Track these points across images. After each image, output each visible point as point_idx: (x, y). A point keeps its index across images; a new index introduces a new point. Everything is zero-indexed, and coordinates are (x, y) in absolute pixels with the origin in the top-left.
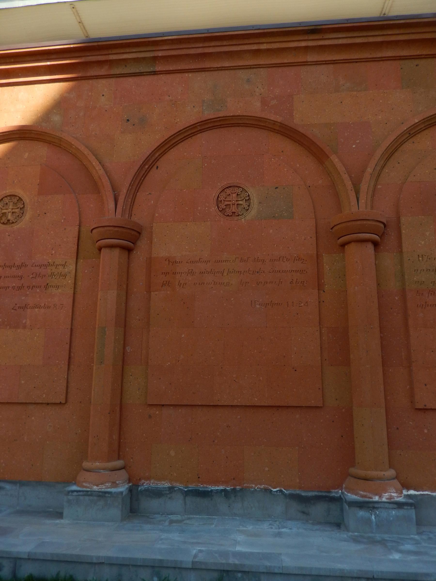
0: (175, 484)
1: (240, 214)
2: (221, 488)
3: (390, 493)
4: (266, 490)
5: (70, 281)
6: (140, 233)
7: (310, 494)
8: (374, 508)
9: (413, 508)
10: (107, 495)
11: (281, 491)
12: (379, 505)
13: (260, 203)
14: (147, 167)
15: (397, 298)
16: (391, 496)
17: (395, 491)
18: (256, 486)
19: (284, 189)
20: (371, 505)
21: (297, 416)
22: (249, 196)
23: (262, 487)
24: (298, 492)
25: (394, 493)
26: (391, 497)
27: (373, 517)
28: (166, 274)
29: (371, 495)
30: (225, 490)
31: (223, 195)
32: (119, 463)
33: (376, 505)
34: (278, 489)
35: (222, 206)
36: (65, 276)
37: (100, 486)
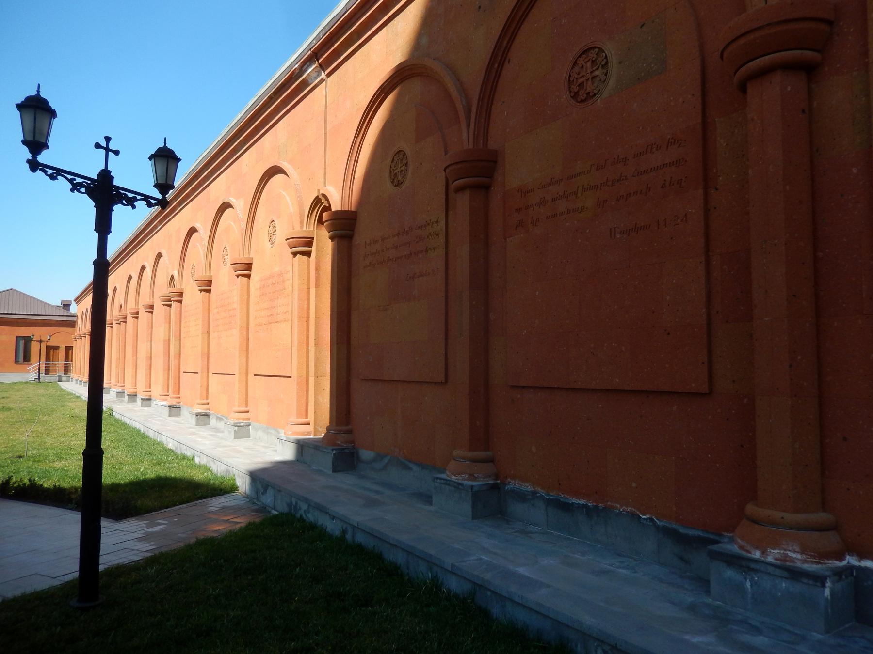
0: (539, 489)
1: (596, 92)
3: (785, 550)
4: (633, 515)
5: (442, 240)
6: (495, 162)
8: (751, 569)
9: (819, 584)
11: (651, 520)
12: (757, 567)
13: (620, 63)
14: (496, 66)
15: (855, 171)
16: (786, 555)
17: (798, 549)
18: (621, 506)
19: (653, 22)
20: (744, 563)
21: (674, 408)
23: (629, 509)
24: (674, 526)
25: (795, 552)
26: (785, 558)
27: (748, 584)
28: (519, 210)
29: (749, 548)
31: (576, 69)
32: (345, 428)
33: (753, 566)
34: (648, 516)
35: (575, 88)
36: (438, 235)
37: (457, 477)
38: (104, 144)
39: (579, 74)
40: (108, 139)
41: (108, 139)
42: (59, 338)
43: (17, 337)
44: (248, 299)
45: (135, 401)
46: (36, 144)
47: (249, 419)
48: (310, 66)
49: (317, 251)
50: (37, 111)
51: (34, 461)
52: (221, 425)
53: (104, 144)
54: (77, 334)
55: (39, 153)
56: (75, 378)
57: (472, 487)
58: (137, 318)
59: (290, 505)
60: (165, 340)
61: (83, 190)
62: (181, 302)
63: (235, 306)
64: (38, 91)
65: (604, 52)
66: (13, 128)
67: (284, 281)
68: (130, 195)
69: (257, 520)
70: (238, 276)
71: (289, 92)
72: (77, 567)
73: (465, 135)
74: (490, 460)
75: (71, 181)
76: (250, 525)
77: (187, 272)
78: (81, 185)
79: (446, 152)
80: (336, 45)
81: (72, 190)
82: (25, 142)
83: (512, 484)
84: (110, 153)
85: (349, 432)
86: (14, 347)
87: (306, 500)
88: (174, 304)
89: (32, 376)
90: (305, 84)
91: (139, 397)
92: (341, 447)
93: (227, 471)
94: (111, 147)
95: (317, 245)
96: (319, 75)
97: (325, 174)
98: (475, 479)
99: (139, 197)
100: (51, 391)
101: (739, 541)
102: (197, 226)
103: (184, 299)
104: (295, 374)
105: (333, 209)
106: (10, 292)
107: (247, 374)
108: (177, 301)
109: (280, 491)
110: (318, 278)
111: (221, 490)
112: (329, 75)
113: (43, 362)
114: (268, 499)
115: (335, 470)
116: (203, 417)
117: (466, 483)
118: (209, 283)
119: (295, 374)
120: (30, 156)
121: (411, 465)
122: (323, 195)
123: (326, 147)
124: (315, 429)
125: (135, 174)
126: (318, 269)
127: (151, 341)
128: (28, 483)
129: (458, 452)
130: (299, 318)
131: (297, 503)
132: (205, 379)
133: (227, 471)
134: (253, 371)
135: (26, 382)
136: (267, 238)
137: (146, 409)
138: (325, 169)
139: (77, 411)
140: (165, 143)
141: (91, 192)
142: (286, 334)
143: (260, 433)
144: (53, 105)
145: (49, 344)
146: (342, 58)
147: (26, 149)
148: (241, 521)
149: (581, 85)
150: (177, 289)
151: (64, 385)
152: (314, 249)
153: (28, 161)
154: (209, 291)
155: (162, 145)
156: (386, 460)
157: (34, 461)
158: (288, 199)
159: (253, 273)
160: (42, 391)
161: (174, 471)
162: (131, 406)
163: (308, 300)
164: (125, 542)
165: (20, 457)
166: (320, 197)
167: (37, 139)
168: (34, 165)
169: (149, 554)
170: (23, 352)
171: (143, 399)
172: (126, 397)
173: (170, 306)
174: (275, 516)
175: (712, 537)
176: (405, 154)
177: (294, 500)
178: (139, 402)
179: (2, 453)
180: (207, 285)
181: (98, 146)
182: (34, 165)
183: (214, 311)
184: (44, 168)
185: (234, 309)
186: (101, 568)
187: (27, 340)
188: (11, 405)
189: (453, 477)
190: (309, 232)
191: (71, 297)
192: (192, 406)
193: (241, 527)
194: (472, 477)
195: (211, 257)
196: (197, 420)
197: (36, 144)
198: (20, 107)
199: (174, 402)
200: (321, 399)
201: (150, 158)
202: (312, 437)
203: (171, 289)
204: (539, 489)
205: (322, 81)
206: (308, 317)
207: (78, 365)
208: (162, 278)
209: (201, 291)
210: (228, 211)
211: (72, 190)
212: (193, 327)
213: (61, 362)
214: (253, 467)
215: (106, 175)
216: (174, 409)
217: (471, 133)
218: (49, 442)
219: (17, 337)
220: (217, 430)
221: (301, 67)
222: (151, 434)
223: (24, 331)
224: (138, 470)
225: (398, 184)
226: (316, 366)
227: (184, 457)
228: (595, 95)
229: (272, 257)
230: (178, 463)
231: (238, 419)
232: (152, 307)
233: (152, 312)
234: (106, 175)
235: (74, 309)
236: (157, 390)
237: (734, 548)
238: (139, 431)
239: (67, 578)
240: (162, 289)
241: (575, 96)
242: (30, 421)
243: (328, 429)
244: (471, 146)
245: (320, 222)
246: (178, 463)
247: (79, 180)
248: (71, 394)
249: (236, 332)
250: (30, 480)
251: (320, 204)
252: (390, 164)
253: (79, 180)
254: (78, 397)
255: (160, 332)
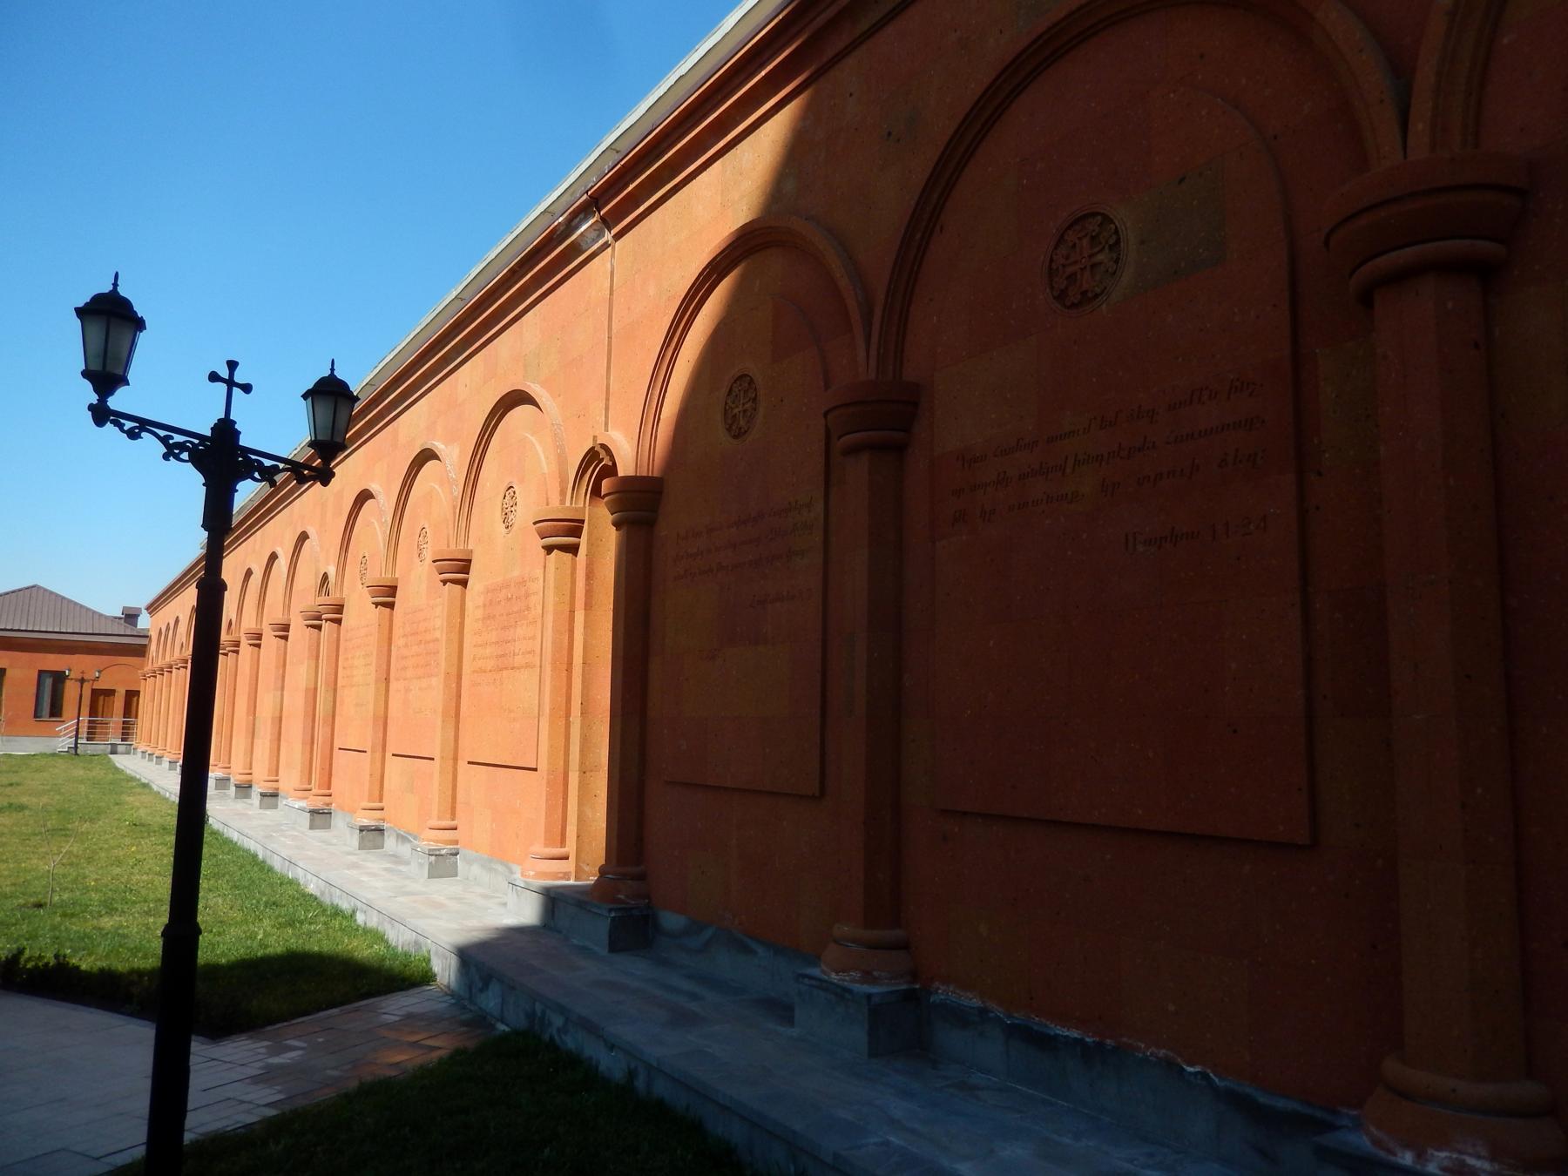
0: (992, 1005)
1: (1098, 290)
2: (1075, 1034)
3: (1460, 1152)
7: (1280, 1103)
10: (847, 996)
11: (1204, 1076)
13: (1142, 242)
14: (918, 236)
16: (1463, 1164)
17: (1484, 1153)
22: (1116, 232)
23: (1162, 1052)
24: (1248, 1090)
25: (1479, 1157)
30: (1079, 1042)
34: (1198, 1069)
38: (225, 374)
39: (1067, 258)
40: (232, 365)
41: (232, 365)
42: (115, 675)
43: (41, 672)
44: (462, 624)
45: (248, 796)
46: (106, 376)
47: (456, 842)
48: (585, 219)
49: (590, 544)
50: (111, 321)
51: (64, 915)
52: (405, 850)
53: (225, 374)
54: (148, 668)
55: (111, 393)
56: (142, 748)
57: (869, 996)
58: (259, 646)
59: (531, 1016)
60: (307, 690)
61: (185, 456)
62: (338, 622)
63: (437, 634)
64: (115, 285)
65: (1112, 221)
66: (69, 348)
67: (527, 596)
68: (268, 463)
69: (471, 1044)
70: (445, 582)
71: (544, 263)
72: (141, 1134)
73: (862, 354)
74: (904, 946)
75: (164, 440)
76: (457, 1056)
77: (352, 569)
78: (182, 447)
79: (827, 387)
80: (631, 187)
81: (166, 457)
82: (86, 374)
83: (943, 993)
84: (236, 390)
85: (641, 877)
86: (33, 690)
87: (562, 1010)
88: (326, 626)
89: (64, 743)
90: (575, 249)
91: (257, 790)
92: (623, 906)
93: (416, 943)
94: (238, 378)
95: (590, 534)
96: (601, 235)
97: (607, 409)
98: (874, 981)
99: (281, 466)
100: (97, 772)
101: (1373, 1129)
102: (374, 487)
103: (344, 616)
104: (543, 766)
105: (621, 473)
106: (33, 592)
107: (455, 759)
108: (332, 620)
109: (513, 988)
110: (589, 593)
111: (404, 980)
112: (618, 237)
113: (85, 719)
114: (490, 1001)
115: (614, 947)
116: (372, 834)
117: (857, 987)
118: (392, 590)
119: (543, 766)
120: (94, 399)
121: (754, 945)
122: (603, 446)
123: (610, 361)
124: (577, 866)
125: (277, 426)
126: (590, 575)
127: (283, 688)
128: (52, 962)
129: (843, 929)
130: (554, 662)
131: (544, 1013)
132: (378, 764)
133: (416, 943)
134: (466, 755)
135: (54, 755)
136: (498, 516)
137: (268, 812)
138: (607, 399)
139: (142, 812)
140: (332, 370)
141: (198, 460)
142: (529, 690)
143: (476, 869)
144: (140, 310)
145: (97, 686)
146: (642, 209)
147: (88, 385)
148: (442, 1046)
149: (1072, 278)
150: (334, 597)
151: (119, 761)
152: (583, 541)
153: (91, 407)
154: (391, 606)
155: (327, 373)
156: (708, 933)
157: (64, 915)
158: (539, 449)
159: (473, 578)
160: (81, 772)
161: (318, 941)
162: (240, 805)
163: (571, 631)
164: (233, 1083)
165: (39, 905)
166: (598, 448)
167: (109, 368)
168: (101, 414)
169: (272, 1112)
170: (50, 700)
171: (263, 795)
172: (233, 789)
173: (319, 628)
174: (504, 1037)
175: (1319, 1114)
176: (751, 381)
177: (538, 1007)
178: (255, 799)
179: (6, 897)
180: (387, 595)
181: (214, 377)
182: (101, 414)
183: (398, 641)
184: (117, 418)
185: (437, 640)
186: (188, 1137)
187: (59, 678)
188: (24, 800)
189: (833, 976)
190: (576, 510)
191: (140, 601)
192: (353, 811)
193: (441, 1059)
194: (867, 977)
195: (397, 544)
196: (362, 839)
197: (106, 376)
198: (81, 312)
199: (319, 803)
200: (589, 813)
201: (305, 396)
202: (572, 882)
203: (323, 599)
204: (992, 1005)
205: (606, 246)
206: (570, 663)
207: (146, 724)
208: (307, 578)
209: (377, 604)
210: (431, 464)
211: (166, 457)
212: (359, 670)
213: (117, 719)
214: (463, 938)
215: (226, 429)
216: (320, 817)
217: (873, 352)
218: (92, 874)
219: (41, 672)
220: (396, 859)
221: (569, 221)
222: (277, 864)
223: (53, 662)
224: (253, 937)
225: (739, 435)
226: (581, 751)
227: (337, 912)
228: (1096, 296)
229: (507, 550)
230: (325, 923)
231: (437, 841)
232: (286, 628)
233: (285, 638)
234: (226, 429)
235: (144, 622)
236: (290, 779)
237: (1361, 1142)
238: (255, 856)
239: (120, 1160)
240: (306, 597)
241: (1061, 296)
242: (62, 832)
243: (603, 871)
244: (872, 376)
245: (596, 492)
246: (325, 923)
247: (178, 438)
248: (132, 779)
249: (437, 682)
250: (57, 956)
251: (597, 463)
252: (725, 396)
253: (178, 438)
254: (145, 786)
255: (299, 674)
